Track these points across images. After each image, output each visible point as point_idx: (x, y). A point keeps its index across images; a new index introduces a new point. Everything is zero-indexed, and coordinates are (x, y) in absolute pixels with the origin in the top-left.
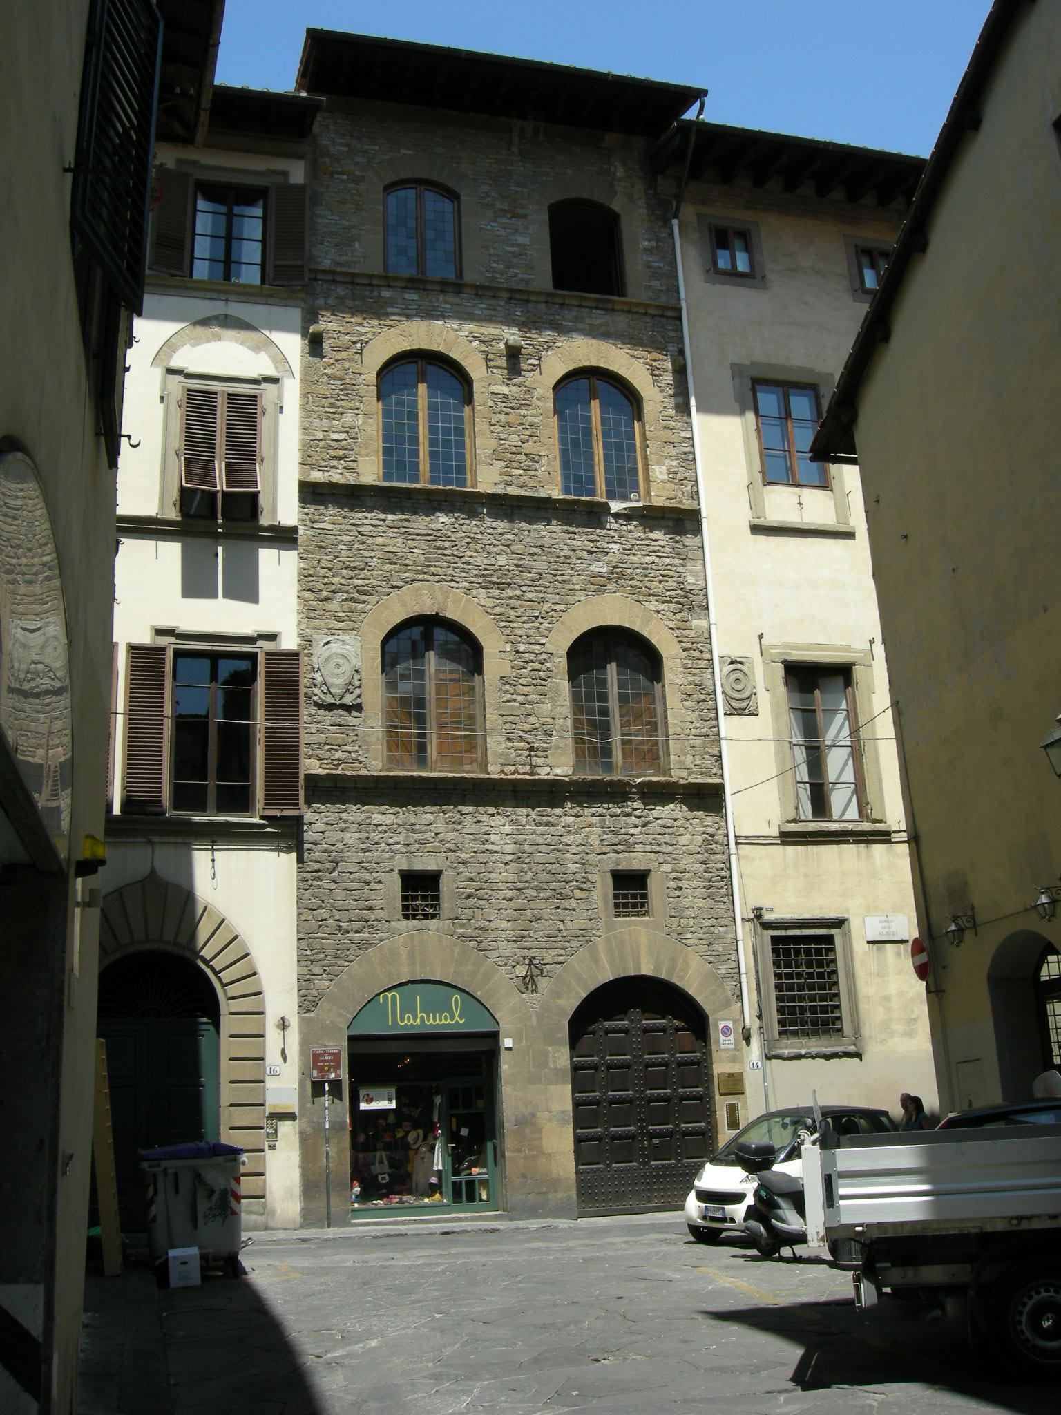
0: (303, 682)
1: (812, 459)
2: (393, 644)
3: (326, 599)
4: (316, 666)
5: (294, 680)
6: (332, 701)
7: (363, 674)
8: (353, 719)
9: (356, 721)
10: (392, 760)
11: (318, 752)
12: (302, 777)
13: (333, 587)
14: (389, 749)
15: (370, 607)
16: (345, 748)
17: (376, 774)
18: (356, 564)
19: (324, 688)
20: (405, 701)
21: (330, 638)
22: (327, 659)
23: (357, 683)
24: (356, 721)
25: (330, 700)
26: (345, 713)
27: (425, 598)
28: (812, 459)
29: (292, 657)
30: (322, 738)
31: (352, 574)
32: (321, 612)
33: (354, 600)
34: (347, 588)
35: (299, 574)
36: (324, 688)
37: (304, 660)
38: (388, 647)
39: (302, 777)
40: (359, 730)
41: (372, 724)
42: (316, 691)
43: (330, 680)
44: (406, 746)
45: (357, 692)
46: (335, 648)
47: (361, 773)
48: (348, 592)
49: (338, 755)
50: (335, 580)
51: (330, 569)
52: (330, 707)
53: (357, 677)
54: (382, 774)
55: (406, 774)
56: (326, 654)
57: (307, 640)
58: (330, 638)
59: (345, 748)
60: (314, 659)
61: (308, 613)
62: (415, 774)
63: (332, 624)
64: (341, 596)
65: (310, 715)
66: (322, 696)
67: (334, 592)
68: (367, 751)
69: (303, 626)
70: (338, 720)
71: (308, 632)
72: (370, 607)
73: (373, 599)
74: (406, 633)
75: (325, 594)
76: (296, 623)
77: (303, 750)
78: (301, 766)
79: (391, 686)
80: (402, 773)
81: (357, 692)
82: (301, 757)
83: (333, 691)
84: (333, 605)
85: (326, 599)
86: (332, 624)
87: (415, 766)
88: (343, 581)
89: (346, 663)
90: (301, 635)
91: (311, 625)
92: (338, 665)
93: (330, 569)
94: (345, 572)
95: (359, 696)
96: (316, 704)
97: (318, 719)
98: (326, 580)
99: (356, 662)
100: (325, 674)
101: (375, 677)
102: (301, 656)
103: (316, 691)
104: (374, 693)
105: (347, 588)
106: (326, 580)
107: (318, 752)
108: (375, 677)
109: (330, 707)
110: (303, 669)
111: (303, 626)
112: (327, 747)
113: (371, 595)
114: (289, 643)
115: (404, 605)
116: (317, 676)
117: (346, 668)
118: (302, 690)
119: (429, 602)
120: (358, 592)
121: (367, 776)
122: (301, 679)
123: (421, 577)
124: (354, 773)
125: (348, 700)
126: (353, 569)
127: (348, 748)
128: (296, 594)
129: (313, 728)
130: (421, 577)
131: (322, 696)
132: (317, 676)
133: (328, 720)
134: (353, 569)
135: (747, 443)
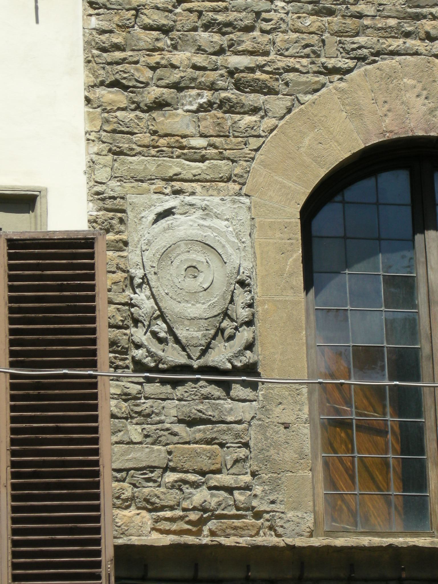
0: (105, 313)
1: (121, 224)
2: (329, 217)
3: (160, 105)
4: (138, 273)
5: (82, 307)
6: (181, 359)
7: (258, 290)
8: (237, 407)
9: (243, 411)
10: (337, 509)
11: (148, 490)
12: (107, 554)
13: (175, 76)
14: (331, 483)
15: (269, 122)
16: (215, 480)
17: (299, 542)
18: (232, 16)
19: (160, 327)
20: (366, 358)
21: (171, 202)
22: (166, 255)
23: (244, 314)
24: (243, 411)
25: (174, 356)
26: (216, 391)
27: (410, 96)
28: (121, 224)
29: (77, 249)
30: (157, 455)
31: (224, 41)
32: (147, 139)
33: (229, 107)
34: (212, 76)
35: (88, 44)
36: (160, 327)
37: (105, 258)
38: (317, 224)
39: (107, 554)
40: (253, 436)
41: (285, 419)
42: (139, 334)
43: (170, 306)
44: (372, 475)
45: (245, 335)
46: (184, 225)
47: (259, 540)
48: (212, 87)
49: (200, 496)
50: (180, 57)
51: (165, 30)
52: (176, 375)
53: (242, 297)
54: (317, 542)
55: (377, 541)
56: (162, 243)
57: (112, 209)
58: (171, 202)
59: (215, 480)
60: (133, 255)
61: (113, 141)
62: (400, 541)
63: (174, 166)
64: (194, 99)
65: (126, 397)
66: (156, 348)
67: (177, 87)
68: (275, 485)
69: (102, 174)
70: (194, 408)
71: (114, 187)
72: (269, 122)
73: (277, 104)
74: (360, 190)
75: (154, 92)
76: (82, 164)
77: (109, 486)
78: (105, 524)
79: (329, 319)
80: (365, 541)
81: (245, 335)
82: (106, 501)
83: (182, 333)
84: (177, 121)
85: (160, 105)
86: (174, 166)
87: (397, 525)
88: (200, 60)
89: (215, 263)
90: (98, 197)
91: (122, 170)
92: (193, 269)
93: (165, 30)
94: (204, 37)
95: (250, 346)
96: (139, 366)
97: (146, 405)
98: (156, 58)
99: (239, 260)
100: (160, 292)
101: (289, 296)
102: (99, 247)
103: (139, 334)
104: (289, 339)
105: (212, 76)
106: (156, 58)
107: (148, 490)
108: (289, 296)
109: (176, 375)
110: (104, 281)
111: (102, 174)
112: (171, 477)
113: (272, 91)
114: (66, 214)
115: (356, 113)
116: (142, 297)
117: (215, 276)
118: (104, 335)
119: (419, 107)
120: (239, 86)
121: (275, 548)
122: (101, 303)
123: (396, 44)
124: (243, 541)
125: (220, 356)
126: (223, 28)
127: (225, 479)
128: (82, 94)
129: (135, 432)
130: (396, 44)
131: (156, 348)
132: (142, 297)
133: (172, 409)
134: (223, 28)
135: (78, 232)
